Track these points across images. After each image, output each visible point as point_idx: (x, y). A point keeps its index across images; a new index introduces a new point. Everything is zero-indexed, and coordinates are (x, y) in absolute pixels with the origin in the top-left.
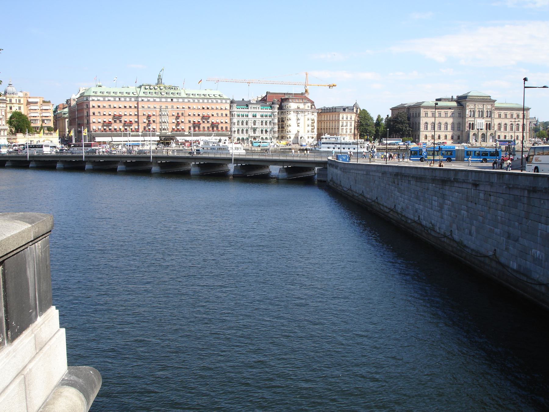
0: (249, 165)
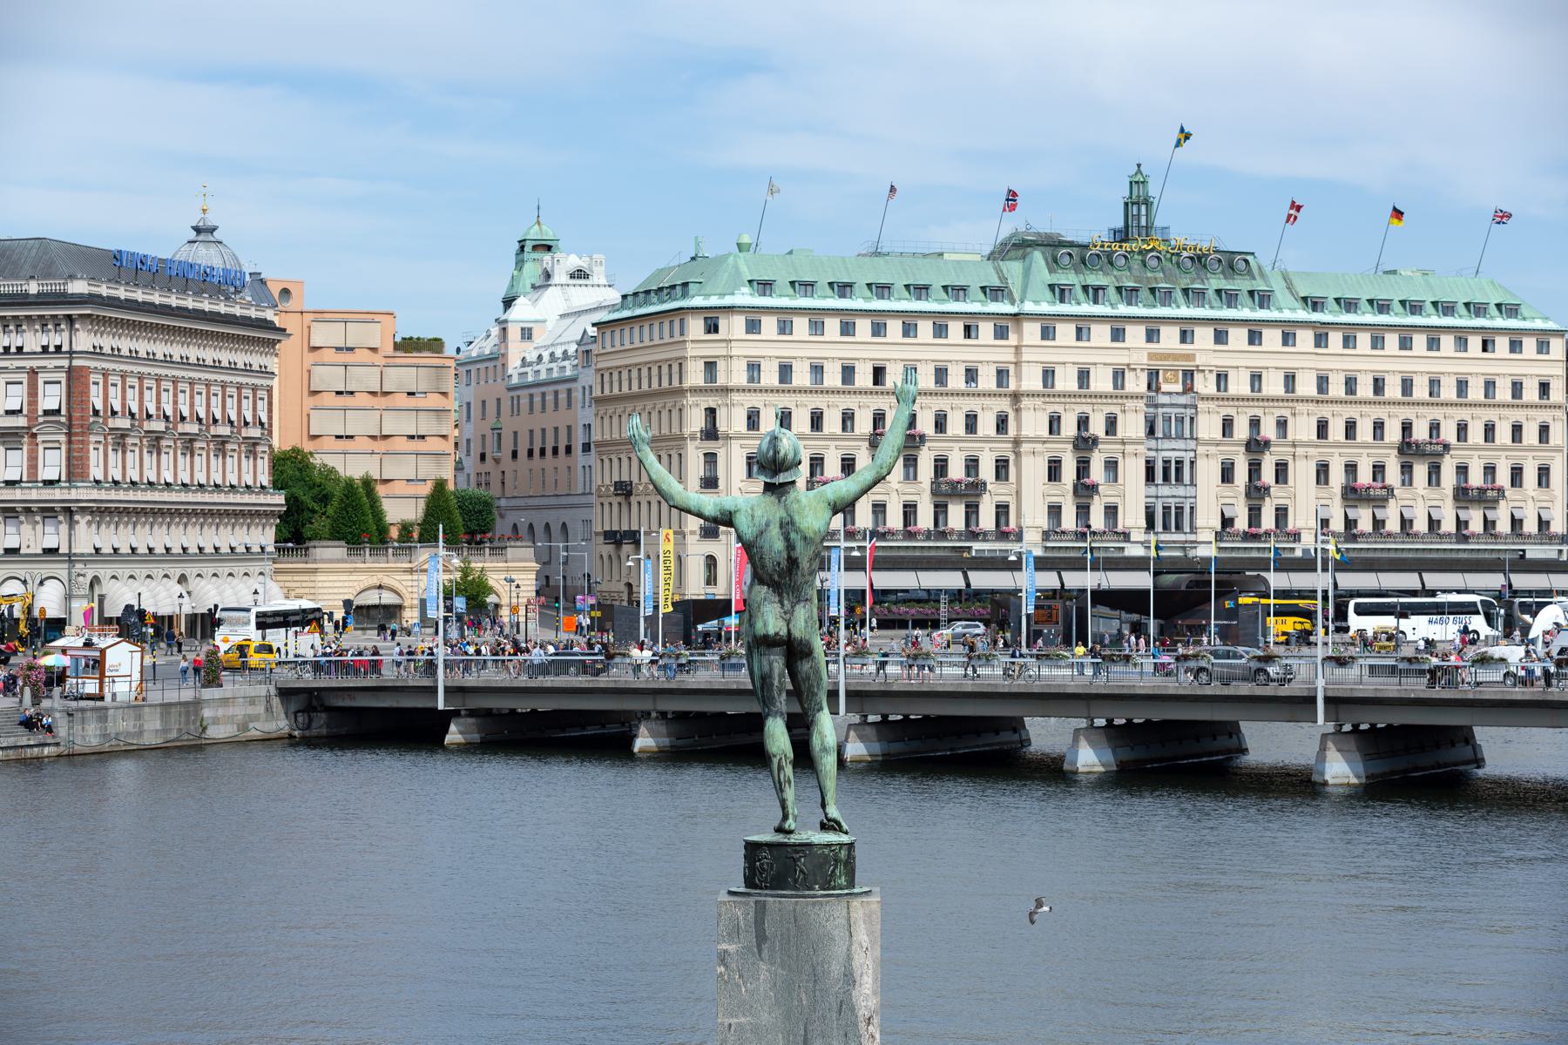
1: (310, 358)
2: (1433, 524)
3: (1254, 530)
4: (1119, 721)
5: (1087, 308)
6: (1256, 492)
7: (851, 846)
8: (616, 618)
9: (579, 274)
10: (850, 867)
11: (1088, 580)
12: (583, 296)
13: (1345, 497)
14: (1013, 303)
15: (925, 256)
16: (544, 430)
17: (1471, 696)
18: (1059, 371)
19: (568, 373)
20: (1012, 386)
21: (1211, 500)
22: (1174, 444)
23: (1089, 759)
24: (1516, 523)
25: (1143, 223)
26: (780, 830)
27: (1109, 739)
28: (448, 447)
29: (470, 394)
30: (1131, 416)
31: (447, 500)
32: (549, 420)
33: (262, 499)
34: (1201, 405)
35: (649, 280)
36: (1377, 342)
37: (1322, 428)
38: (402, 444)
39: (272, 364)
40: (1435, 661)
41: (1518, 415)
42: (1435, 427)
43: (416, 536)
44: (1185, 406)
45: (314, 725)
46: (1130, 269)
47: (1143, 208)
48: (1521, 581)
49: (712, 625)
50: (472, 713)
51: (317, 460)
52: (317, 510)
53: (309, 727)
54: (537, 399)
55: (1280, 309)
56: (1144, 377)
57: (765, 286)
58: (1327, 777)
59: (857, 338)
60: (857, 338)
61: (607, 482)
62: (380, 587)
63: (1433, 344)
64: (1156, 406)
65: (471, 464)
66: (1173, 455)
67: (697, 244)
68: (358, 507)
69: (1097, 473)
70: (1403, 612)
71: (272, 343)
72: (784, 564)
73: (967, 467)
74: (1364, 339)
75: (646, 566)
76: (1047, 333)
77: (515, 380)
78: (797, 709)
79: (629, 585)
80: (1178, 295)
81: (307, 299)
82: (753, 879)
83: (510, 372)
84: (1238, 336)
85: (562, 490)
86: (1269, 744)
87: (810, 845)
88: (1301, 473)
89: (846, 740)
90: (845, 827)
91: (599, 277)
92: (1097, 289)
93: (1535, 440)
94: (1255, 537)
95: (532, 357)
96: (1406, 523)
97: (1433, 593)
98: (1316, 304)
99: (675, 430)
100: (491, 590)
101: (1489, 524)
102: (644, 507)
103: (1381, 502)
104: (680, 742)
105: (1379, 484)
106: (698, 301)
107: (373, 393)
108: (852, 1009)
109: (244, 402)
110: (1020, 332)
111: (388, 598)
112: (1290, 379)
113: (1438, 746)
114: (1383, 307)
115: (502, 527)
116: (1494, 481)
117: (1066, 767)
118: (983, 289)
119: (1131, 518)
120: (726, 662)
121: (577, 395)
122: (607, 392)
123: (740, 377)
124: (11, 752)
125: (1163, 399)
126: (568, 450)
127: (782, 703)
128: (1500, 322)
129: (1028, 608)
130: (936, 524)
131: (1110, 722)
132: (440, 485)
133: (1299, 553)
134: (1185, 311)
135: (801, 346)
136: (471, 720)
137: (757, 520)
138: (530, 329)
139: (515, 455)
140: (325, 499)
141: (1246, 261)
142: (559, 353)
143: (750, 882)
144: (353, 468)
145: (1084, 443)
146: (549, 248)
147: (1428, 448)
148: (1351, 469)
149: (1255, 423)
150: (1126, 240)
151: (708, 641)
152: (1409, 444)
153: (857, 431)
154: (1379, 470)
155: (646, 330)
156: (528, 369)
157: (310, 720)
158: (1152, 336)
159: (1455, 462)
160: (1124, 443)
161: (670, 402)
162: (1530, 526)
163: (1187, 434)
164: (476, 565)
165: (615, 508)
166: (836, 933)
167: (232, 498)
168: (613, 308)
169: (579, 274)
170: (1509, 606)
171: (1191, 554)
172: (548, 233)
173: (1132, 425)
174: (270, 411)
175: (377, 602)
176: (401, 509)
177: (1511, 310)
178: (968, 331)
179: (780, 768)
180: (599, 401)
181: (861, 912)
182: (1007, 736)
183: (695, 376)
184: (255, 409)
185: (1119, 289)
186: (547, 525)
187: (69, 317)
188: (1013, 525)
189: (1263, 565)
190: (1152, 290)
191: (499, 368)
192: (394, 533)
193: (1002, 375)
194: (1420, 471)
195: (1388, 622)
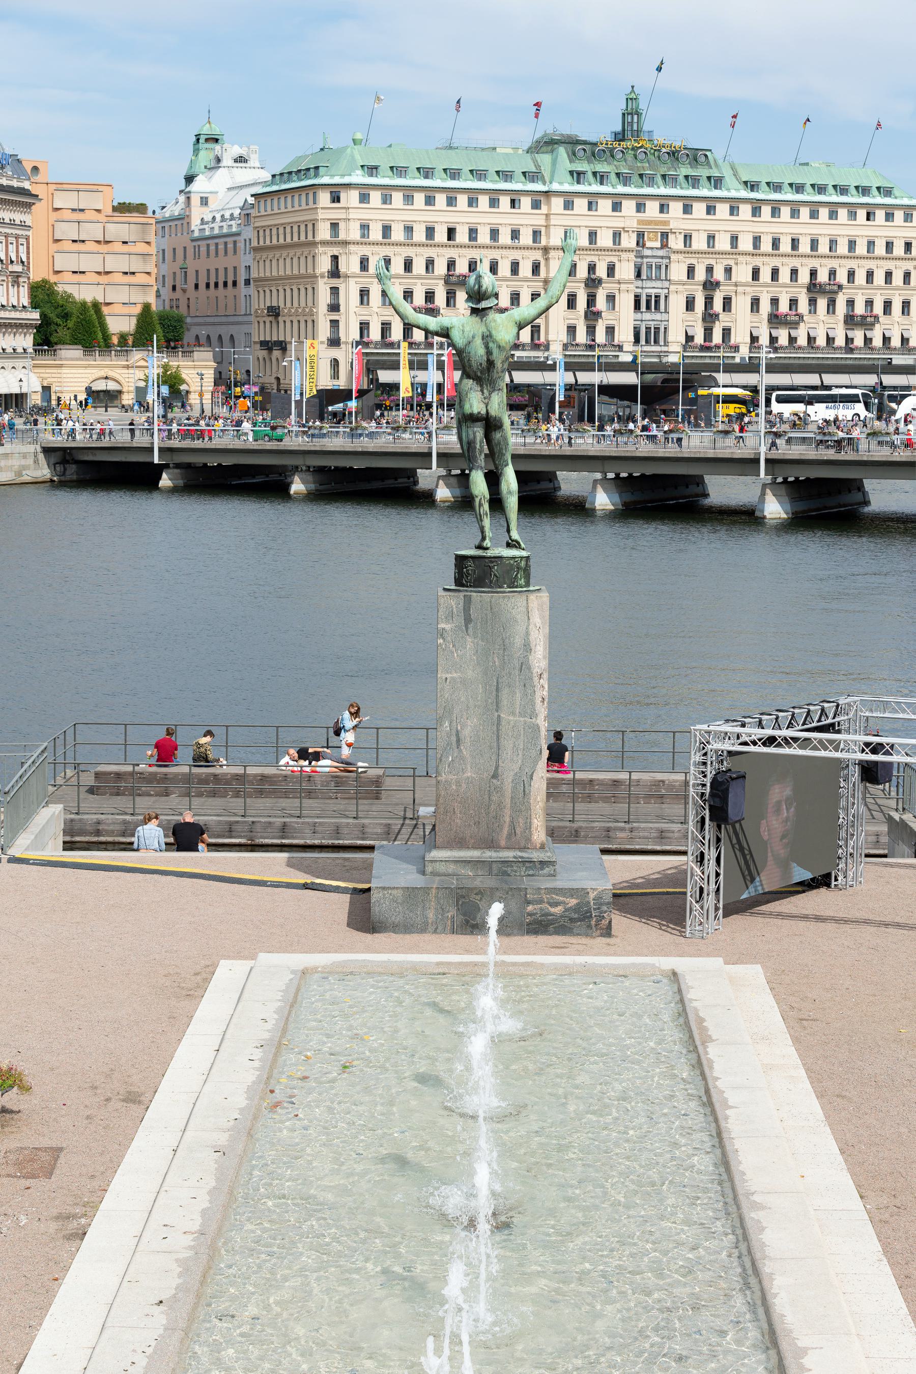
0: (655, 477)
1: (54, 216)
2: (830, 340)
3: (708, 344)
4: (624, 475)
5: (596, 188)
6: (709, 318)
7: (528, 558)
8: (272, 399)
9: (240, 159)
10: (527, 572)
11: (595, 378)
12: (244, 175)
13: (770, 321)
14: (544, 183)
15: (483, 149)
16: (217, 270)
17: (865, 459)
18: (694, 235)
19: (234, 229)
20: (544, 242)
21: (679, 323)
22: (654, 284)
23: (603, 501)
24: (886, 340)
25: (635, 128)
26: (480, 547)
27: (617, 486)
28: (151, 280)
29: (165, 244)
31: (151, 318)
32: (221, 262)
33: (24, 315)
34: (673, 257)
35: (290, 164)
36: (795, 213)
37: (756, 274)
38: (119, 278)
39: (28, 219)
40: (841, 435)
41: (871, 264)
42: (833, 273)
43: (130, 343)
44: (662, 257)
45: (68, 473)
46: (625, 160)
47: (635, 117)
48: (889, 380)
49: (339, 407)
50: (178, 466)
51: (60, 288)
52: (62, 324)
53: (64, 474)
54: (212, 248)
55: (728, 190)
56: (634, 237)
57: (372, 170)
58: (766, 513)
59: (501, 210)
60: (437, 207)
61: (262, 306)
62: (106, 378)
63: (833, 215)
64: (642, 257)
65: (166, 292)
66: (653, 292)
67: (325, 139)
68: (89, 322)
69: (601, 303)
70: (810, 401)
71: (29, 205)
72: (484, 364)
73: (512, 298)
74: (785, 211)
75: (296, 365)
76: (568, 205)
77: (196, 234)
78: (492, 467)
79: (278, 379)
80: (659, 179)
81: (48, 174)
82: (460, 581)
83: (193, 228)
84: (699, 209)
85: (230, 311)
86: (722, 490)
87: (500, 557)
88: (741, 304)
89: (437, 486)
90: (523, 545)
91: (254, 161)
92: (579, 174)
93: (422, 271)
94: (708, 349)
95: (208, 218)
96: (811, 340)
97: (829, 388)
98: (752, 186)
99: (310, 271)
100: (183, 382)
101: (868, 340)
102: (288, 324)
103: (794, 325)
104: (322, 487)
105: (794, 313)
107: (98, 242)
108: (529, 668)
109: (21, 247)
110: (549, 204)
111: (112, 386)
112: (734, 240)
113: (840, 493)
114: (798, 188)
115: (188, 337)
116: (872, 311)
117: (587, 506)
118: (524, 173)
119: (624, 335)
120: (354, 432)
121: (241, 245)
122: (262, 243)
123: (354, 234)
125: (647, 252)
126: (235, 284)
127: (481, 460)
128: (879, 200)
129: (560, 397)
130: (532, 339)
131: (617, 475)
132: (147, 307)
133: (737, 360)
134: (663, 191)
135: (398, 213)
136: (177, 471)
137: (466, 334)
138: (207, 198)
139: (197, 286)
140: (66, 316)
141: (706, 156)
142: (227, 216)
143: (459, 582)
144: (85, 293)
145: (592, 283)
146: (217, 140)
147: (828, 287)
148: (775, 302)
149: (710, 270)
150: (623, 140)
151: (339, 418)
152: (815, 285)
153: (436, 273)
154: (793, 302)
155: (275, 201)
156: (205, 226)
157: (65, 469)
158: (640, 208)
159: (845, 298)
160: (619, 283)
161: (306, 251)
162: (896, 342)
163: (663, 277)
164: (174, 364)
165: (268, 325)
166: (519, 617)
167: (14, 315)
168: (265, 184)
169: (240, 159)
170: (881, 397)
171: (664, 360)
172: (216, 130)
173: (626, 271)
174: (28, 253)
175: (104, 388)
176: (120, 323)
177: (886, 191)
178: (513, 203)
179: (480, 505)
180: (256, 250)
181: (536, 603)
182: (545, 485)
183: (324, 233)
184: (17, 251)
185: (618, 175)
186: (220, 336)
188: (542, 339)
189: (716, 368)
190: (641, 176)
191: (185, 225)
192: (115, 340)
193: (536, 234)
194: (822, 303)
195: (799, 407)
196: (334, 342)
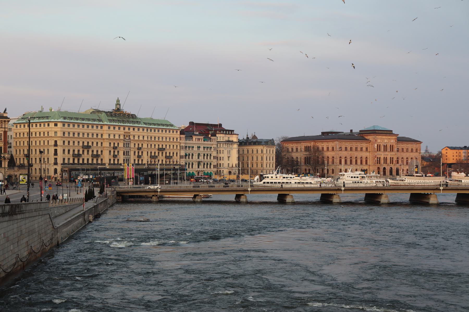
30: (105, 143)
106: (53, 120)
124: (27, 216)
158: (124, 129)
187: (5, 121)
196: (56, 163)
